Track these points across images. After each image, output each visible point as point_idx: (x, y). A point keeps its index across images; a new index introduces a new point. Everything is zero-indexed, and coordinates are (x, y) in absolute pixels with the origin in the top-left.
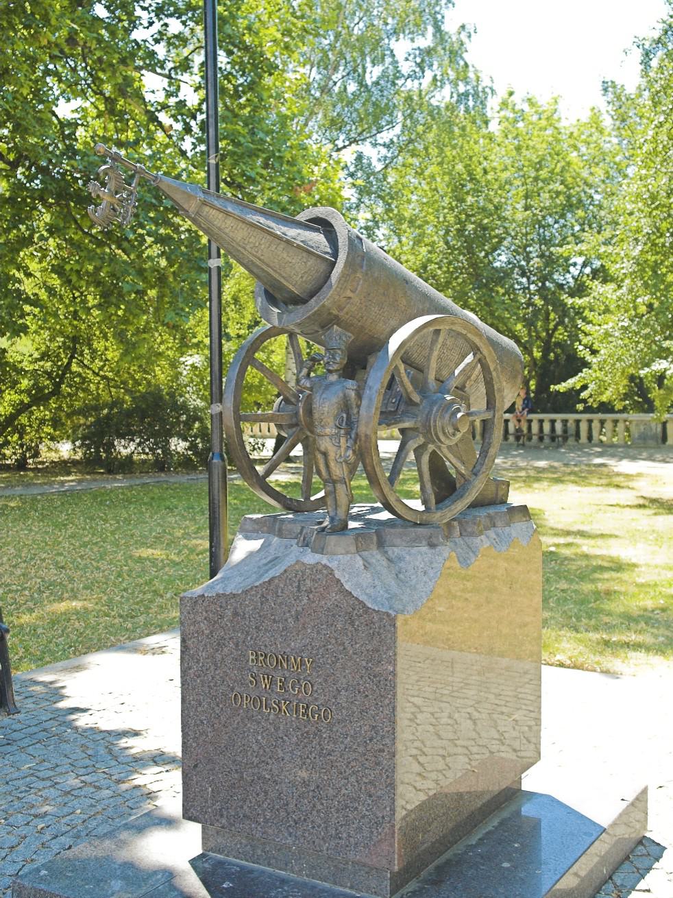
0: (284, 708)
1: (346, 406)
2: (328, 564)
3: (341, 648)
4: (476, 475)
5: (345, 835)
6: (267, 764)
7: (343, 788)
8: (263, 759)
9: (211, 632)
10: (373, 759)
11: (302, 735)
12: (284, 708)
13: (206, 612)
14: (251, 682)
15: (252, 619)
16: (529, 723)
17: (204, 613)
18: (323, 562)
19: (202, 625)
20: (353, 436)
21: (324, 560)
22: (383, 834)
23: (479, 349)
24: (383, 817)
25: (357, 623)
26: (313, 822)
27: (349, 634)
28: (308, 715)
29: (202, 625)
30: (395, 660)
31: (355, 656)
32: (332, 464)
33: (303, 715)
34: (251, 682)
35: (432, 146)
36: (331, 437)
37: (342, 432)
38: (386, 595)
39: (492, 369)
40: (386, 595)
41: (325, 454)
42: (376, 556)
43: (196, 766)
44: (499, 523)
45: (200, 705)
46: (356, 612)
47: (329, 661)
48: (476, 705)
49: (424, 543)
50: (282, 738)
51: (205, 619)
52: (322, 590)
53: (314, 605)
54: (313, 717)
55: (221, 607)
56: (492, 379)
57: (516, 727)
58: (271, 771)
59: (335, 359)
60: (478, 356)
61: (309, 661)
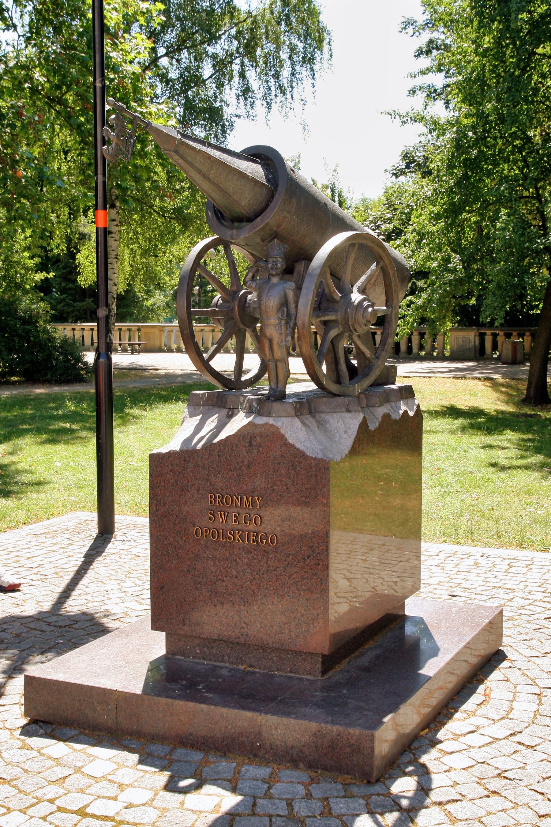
0: (237, 536)
1: (285, 303)
2: (274, 424)
3: (285, 488)
4: (378, 358)
5: (287, 631)
6: (223, 581)
7: (286, 595)
8: (220, 577)
9: (176, 481)
10: (310, 571)
11: (253, 557)
12: (237, 536)
13: (172, 465)
14: (210, 519)
15: (211, 469)
16: (395, 580)
17: (170, 466)
18: (271, 423)
19: (168, 476)
20: (291, 325)
21: (271, 421)
22: (318, 628)
23: (382, 259)
24: (318, 615)
25: (298, 468)
26: (261, 623)
27: (292, 477)
28: (257, 541)
29: (168, 476)
30: (329, 495)
31: (296, 494)
32: (275, 347)
33: (254, 541)
34: (210, 519)
35: (484, 223)
36: (275, 326)
37: (283, 322)
38: (320, 447)
39: (391, 275)
40: (320, 447)
41: (271, 341)
42: (310, 420)
43: (163, 587)
44: (393, 398)
45: (166, 539)
46: (297, 460)
47: (275, 499)
48: (349, 568)
49: (344, 409)
50: (236, 560)
51: (171, 470)
52: (269, 444)
53: (263, 456)
54: (262, 542)
55: (185, 461)
56: (391, 282)
57: (384, 583)
58: (226, 586)
59: (276, 265)
60: (381, 264)
61: (258, 499)
